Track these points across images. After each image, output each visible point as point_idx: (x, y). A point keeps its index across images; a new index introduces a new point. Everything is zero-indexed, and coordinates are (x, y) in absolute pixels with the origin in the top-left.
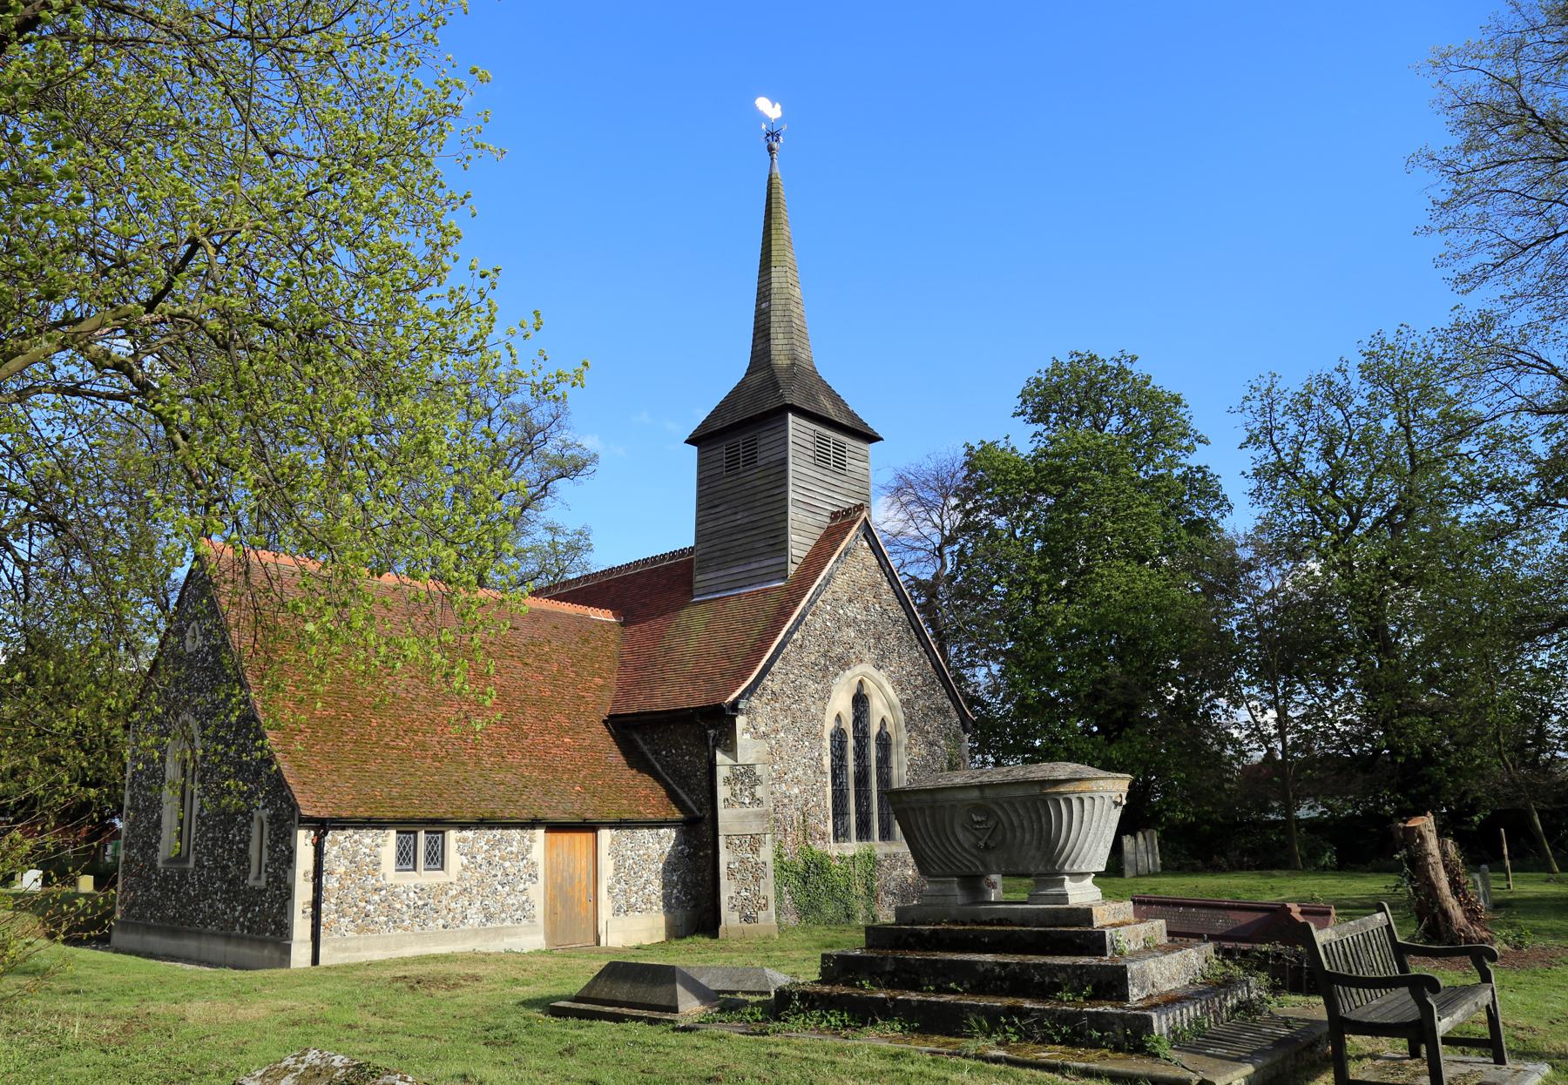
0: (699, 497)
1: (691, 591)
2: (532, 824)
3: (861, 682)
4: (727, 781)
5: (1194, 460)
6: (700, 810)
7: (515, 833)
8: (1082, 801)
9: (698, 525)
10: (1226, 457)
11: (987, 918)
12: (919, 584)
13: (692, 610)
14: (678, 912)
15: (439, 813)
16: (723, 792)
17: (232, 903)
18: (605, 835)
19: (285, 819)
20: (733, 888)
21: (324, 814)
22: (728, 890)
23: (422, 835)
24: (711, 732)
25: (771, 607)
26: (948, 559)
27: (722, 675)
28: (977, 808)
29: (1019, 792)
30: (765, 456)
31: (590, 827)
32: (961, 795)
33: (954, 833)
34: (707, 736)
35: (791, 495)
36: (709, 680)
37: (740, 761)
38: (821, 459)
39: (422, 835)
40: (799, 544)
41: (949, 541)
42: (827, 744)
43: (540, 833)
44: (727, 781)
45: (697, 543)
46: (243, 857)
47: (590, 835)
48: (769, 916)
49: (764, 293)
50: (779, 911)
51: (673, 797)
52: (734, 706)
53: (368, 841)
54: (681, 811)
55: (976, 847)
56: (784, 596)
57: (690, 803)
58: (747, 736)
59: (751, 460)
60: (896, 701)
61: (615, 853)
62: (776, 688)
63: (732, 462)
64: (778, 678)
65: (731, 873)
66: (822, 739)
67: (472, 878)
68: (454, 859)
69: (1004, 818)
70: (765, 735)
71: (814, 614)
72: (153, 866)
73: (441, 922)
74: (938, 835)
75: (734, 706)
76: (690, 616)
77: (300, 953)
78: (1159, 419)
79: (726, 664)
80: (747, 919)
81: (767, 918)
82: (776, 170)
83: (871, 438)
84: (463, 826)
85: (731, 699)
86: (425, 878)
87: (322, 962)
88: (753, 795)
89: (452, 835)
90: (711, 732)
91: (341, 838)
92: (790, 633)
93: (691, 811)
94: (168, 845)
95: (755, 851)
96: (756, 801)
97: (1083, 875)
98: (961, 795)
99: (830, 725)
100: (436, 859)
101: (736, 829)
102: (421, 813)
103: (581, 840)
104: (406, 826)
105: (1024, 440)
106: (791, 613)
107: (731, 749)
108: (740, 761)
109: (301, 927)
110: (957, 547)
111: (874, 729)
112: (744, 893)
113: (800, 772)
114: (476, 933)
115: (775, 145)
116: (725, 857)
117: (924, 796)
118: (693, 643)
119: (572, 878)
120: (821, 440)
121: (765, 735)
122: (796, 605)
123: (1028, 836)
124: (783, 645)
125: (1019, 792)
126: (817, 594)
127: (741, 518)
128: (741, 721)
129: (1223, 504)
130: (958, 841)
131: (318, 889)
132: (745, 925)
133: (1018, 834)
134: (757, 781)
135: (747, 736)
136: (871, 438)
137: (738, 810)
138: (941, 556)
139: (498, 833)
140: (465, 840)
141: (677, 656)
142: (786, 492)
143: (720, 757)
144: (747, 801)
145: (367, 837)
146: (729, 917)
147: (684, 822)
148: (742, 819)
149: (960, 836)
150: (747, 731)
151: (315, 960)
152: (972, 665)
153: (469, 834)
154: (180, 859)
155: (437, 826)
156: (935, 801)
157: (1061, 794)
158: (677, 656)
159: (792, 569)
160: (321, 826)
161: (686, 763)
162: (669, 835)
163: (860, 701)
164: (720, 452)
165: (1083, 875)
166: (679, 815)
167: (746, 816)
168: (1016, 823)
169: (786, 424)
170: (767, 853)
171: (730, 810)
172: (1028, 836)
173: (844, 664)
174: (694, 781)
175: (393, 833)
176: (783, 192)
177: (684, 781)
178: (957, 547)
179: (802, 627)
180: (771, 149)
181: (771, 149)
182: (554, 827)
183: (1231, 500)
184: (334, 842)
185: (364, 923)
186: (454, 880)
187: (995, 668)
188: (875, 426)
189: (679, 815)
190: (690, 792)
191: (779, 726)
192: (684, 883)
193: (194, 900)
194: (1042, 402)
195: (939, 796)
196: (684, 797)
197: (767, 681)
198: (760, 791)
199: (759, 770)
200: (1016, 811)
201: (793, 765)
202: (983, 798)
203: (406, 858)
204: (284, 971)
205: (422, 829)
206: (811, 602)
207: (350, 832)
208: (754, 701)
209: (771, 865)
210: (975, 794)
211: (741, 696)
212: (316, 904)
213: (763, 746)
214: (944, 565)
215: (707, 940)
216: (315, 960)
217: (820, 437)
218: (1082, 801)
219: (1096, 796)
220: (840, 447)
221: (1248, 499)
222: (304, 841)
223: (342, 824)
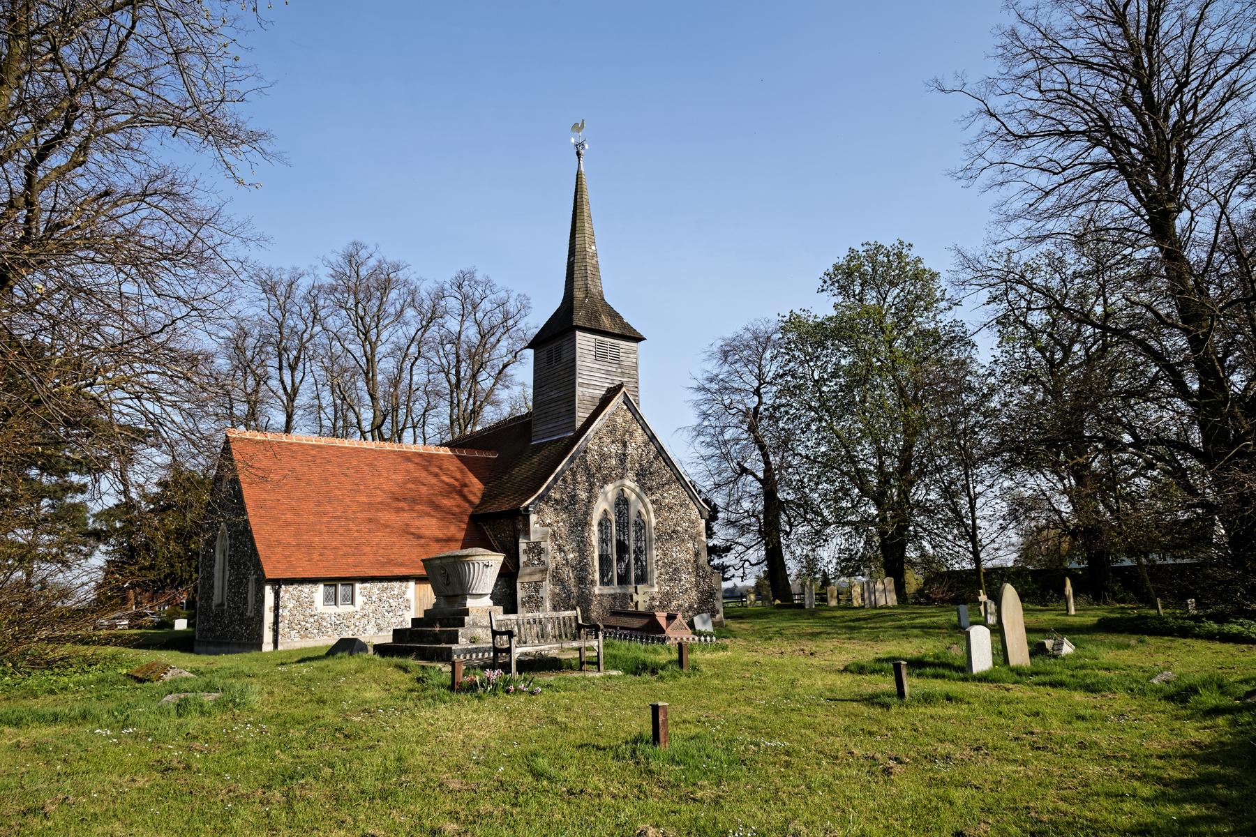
2: (314, 581)
7: (396, 584)
10: (972, 314)
16: (523, 558)
17: (229, 624)
19: (262, 581)
30: (565, 357)
40: (581, 415)
43: (412, 584)
44: (525, 552)
46: (246, 603)
59: (559, 359)
65: (524, 604)
68: (359, 599)
72: (210, 606)
77: (267, 646)
83: (639, 339)
84: (364, 580)
86: (344, 609)
89: (358, 586)
94: (216, 599)
97: (481, 595)
104: (330, 582)
105: (824, 307)
107: (527, 533)
109: (268, 636)
115: (582, 152)
128: (533, 518)
131: (276, 616)
136: (639, 339)
139: (385, 584)
145: (306, 588)
153: (368, 585)
154: (222, 604)
160: (277, 583)
165: (481, 595)
175: (321, 586)
176: (587, 184)
180: (578, 154)
181: (578, 154)
184: (286, 591)
193: (227, 626)
194: (845, 276)
199: (543, 545)
203: (327, 599)
204: (254, 654)
212: (276, 623)
222: (269, 592)
223: (290, 582)
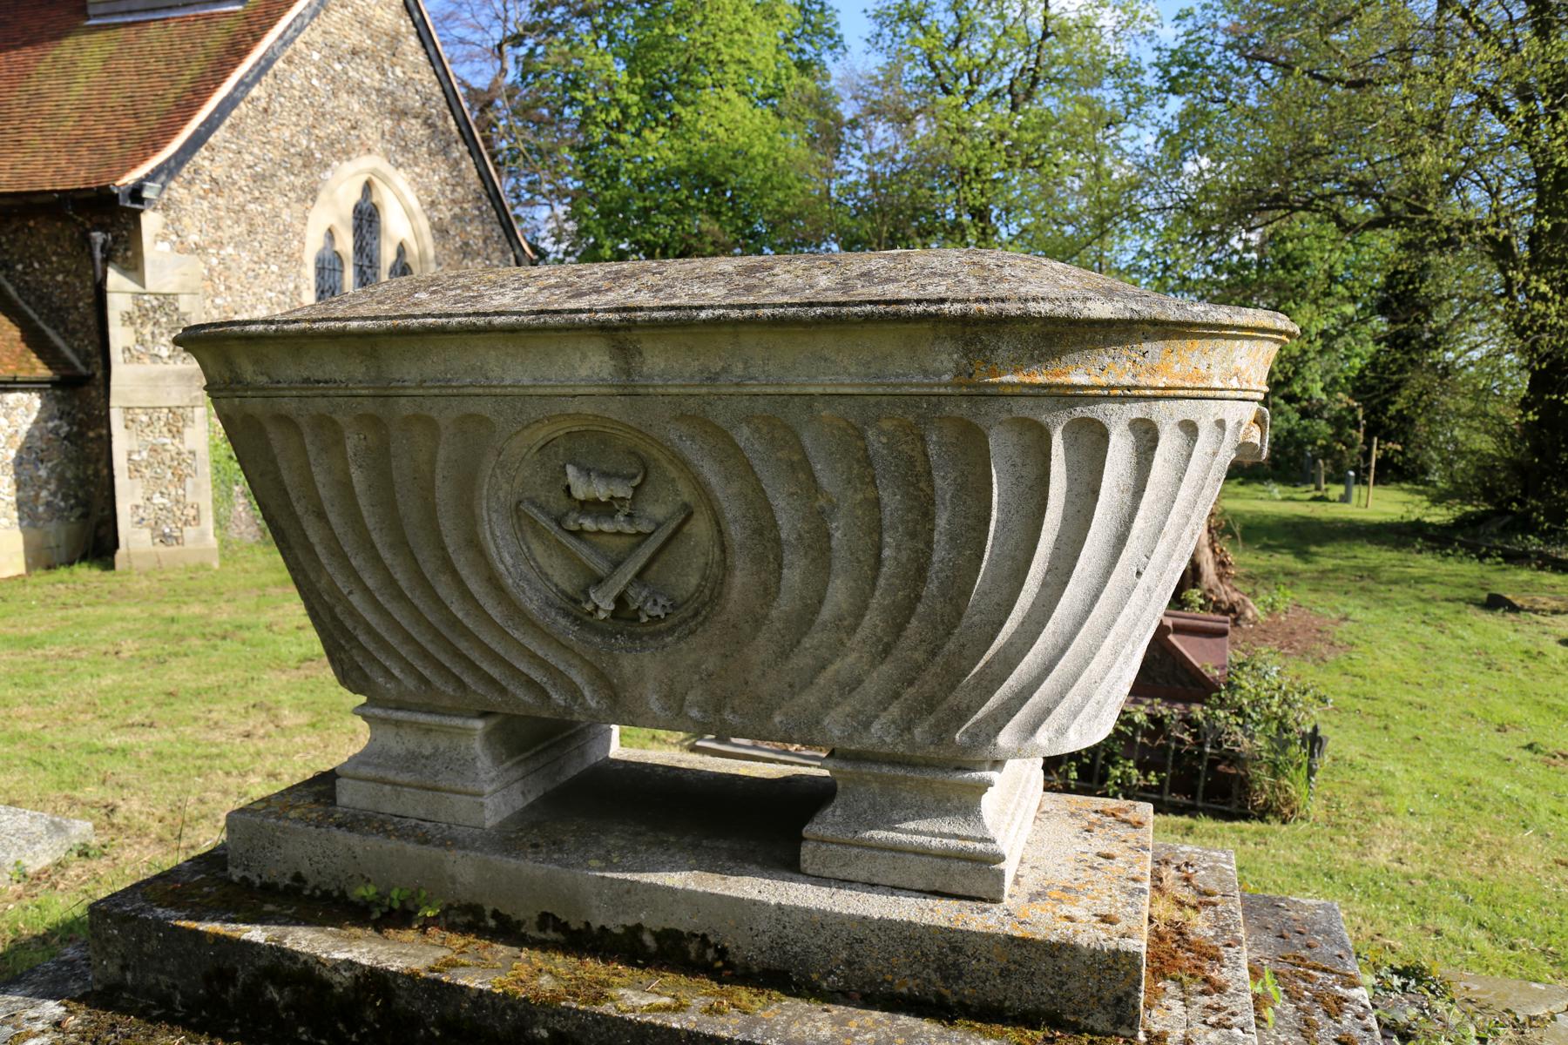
1: (85, 8)
3: (368, 187)
4: (128, 319)
6: (87, 365)
8: (1146, 436)
11: (617, 923)
12: (473, 93)
13: (84, 39)
14: (53, 526)
16: (120, 336)
20: (139, 492)
22: (129, 496)
24: (98, 237)
25: (217, 40)
26: (510, 64)
27: (121, 141)
28: (587, 443)
29: (837, 372)
32: (513, 370)
33: (474, 544)
34: (87, 242)
36: (100, 149)
41: (517, 40)
42: (310, 272)
44: (128, 319)
48: (203, 535)
50: (220, 523)
51: (35, 340)
52: (136, 193)
54: (49, 365)
55: (573, 606)
56: (238, 26)
57: (68, 352)
58: (165, 247)
62: (219, 173)
64: (223, 158)
65: (135, 469)
66: (300, 262)
69: (726, 493)
70: (198, 249)
71: (289, 61)
74: (402, 544)
75: (136, 193)
76: (80, 48)
79: (130, 125)
80: (165, 539)
81: (203, 537)
85: (130, 178)
90: (98, 237)
92: (244, 85)
93: (68, 364)
95: (177, 433)
98: (513, 370)
99: (314, 244)
101: (141, 397)
106: (247, 52)
107: (134, 267)
110: (523, 51)
111: (388, 255)
112: (157, 499)
116: (122, 443)
117: (334, 367)
118: (79, 89)
121: (198, 249)
122: (257, 39)
123: (839, 593)
124: (230, 103)
125: (837, 372)
126: (298, 28)
128: (151, 222)
129: (835, 42)
130: (494, 582)
132: (162, 548)
133: (793, 576)
135: (165, 247)
137: (148, 368)
138: (501, 56)
141: (47, 107)
143: (114, 278)
146: (132, 536)
147: (54, 384)
148: (154, 381)
149: (505, 559)
152: (531, 203)
156: (386, 394)
157: (1069, 396)
158: (47, 107)
161: (57, 285)
162: (34, 401)
163: (366, 218)
167: (162, 377)
168: (788, 523)
171: (135, 368)
172: (839, 593)
173: (341, 149)
174: (74, 316)
177: (57, 316)
178: (523, 51)
179: (267, 79)
183: (846, 41)
187: (560, 210)
189: (43, 371)
190: (68, 334)
191: (224, 235)
192: (62, 480)
195: (407, 370)
196: (58, 341)
197: (201, 157)
200: (801, 467)
201: (250, 300)
202: (630, 393)
206: (285, 41)
208: (176, 189)
210: (593, 365)
211: (152, 176)
213: (197, 266)
214: (504, 71)
215: (96, 572)
218: (1146, 436)
219: (1167, 416)
221: (865, 46)
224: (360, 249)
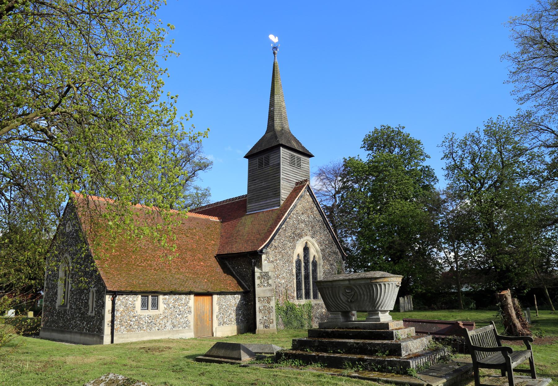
0: (249, 177)
1: (246, 210)
2: (189, 293)
3: (306, 243)
4: (259, 278)
5: (425, 164)
6: (249, 288)
7: (183, 297)
8: (385, 285)
9: (248, 187)
10: (436, 163)
11: (351, 327)
12: (327, 208)
13: (246, 217)
14: (241, 325)
15: (156, 289)
16: (257, 282)
17: (82, 321)
18: (215, 297)
19: (102, 291)
20: (261, 316)
21: (115, 290)
22: (259, 317)
23: (150, 297)
24: (253, 260)
25: (274, 216)
26: (337, 199)
27: (257, 240)
28: (348, 287)
29: (363, 282)
30: (272, 162)
31: (210, 294)
32: (342, 283)
33: (339, 296)
34: (251, 262)
35: (282, 176)
36: (252, 242)
37: (263, 271)
38: (292, 163)
39: (150, 297)
40: (284, 194)
41: (338, 192)
42: (294, 265)
43: (192, 296)
44: (259, 278)
45: (248, 193)
46: (86, 305)
47: (210, 297)
48: (274, 326)
49: (272, 104)
50: (277, 324)
51: (240, 283)
52: (261, 251)
53: (131, 299)
54: (242, 288)
55: (347, 301)
56: (279, 212)
57: (245, 286)
58: (266, 262)
59: (267, 164)
60: (319, 249)
61: (219, 304)
62: (276, 245)
63: (261, 164)
64: (277, 241)
65: (260, 311)
66: (292, 263)
67: (168, 312)
68: (162, 306)
69: (357, 291)
70: (272, 262)
71: (290, 219)
72: (55, 308)
73: (157, 328)
74: (334, 297)
75: (261, 251)
76: (246, 219)
77: (107, 339)
78: (413, 149)
79: (258, 236)
80: (266, 327)
81: (273, 327)
82: (276, 60)
83: (310, 156)
84: (165, 294)
85: (260, 249)
86: (151, 312)
87: (115, 342)
88: (268, 283)
89: (161, 297)
90: (253, 260)
91: (121, 298)
92: (281, 225)
93: (246, 289)
94: (60, 301)
95: (269, 303)
96: (269, 285)
97: (386, 311)
98: (342, 283)
99: (295, 258)
100: (155, 306)
101: (262, 295)
102: (150, 289)
103: (207, 299)
104: (145, 294)
105: (364, 156)
106: (282, 218)
107: (260, 267)
108: (263, 271)
109: (107, 330)
110: (340, 195)
111: (311, 259)
112: (265, 318)
113: (285, 275)
114: (169, 332)
115: (276, 52)
116: (258, 305)
117: (329, 283)
118: (247, 229)
119: (203, 312)
120: (292, 156)
121: (272, 262)
122: (283, 215)
123: (366, 297)
124: (278, 229)
125: (363, 282)
126: (291, 211)
127: (264, 184)
128: (264, 257)
129: (435, 179)
130: (341, 299)
131: (113, 316)
132: (265, 329)
133: (362, 297)
134: (269, 278)
135: (266, 262)
136: (310, 156)
137: (263, 288)
138: (335, 198)
139: (177, 296)
140: (165, 299)
141: (241, 233)
142: (280, 175)
143: (256, 269)
144: (266, 285)
145: (131, 298)
146: (260, 326)
147: (243, 293)
148: (264, 291)
149: (342, 298)
150: (266, 260)
151: (112, 341)
152: (346, 237)
153: (167, 297)
154: (64, 305)
155: (156, 294)
156: (333, 285)
157: (377, 282)
158: (241, 233)
159: (282, 202)
160: (114, 294)
161: (244, 271)
162: (238, 297)
163: (306, 249)
164: (256, 161)
165: (386, 311)
166: (242, 290)
167: (266, 290)
168: (362, 293)
169: (280, 151)
170: (273, 304)
171: (260, 288)
172: (366, 297)
173: (300, 236)
174: (247, 278)
175: (140, 296)
176: (279, 68)
177: (243, 278)
178: (340, 195)
179: (286, 223)
180: (274, 53)
181: (274, 53)
182: (197, 294)
183: (438, 178)
184: (119, 300)
185: (130, 328)
186: (162, 313)
187: (354, 238)
188: (311, 152)
189: (242, 290)
190: (246, 282)
191: (277, 258)
192: (243, 314)
193: (69, 320)
194: (371, 143)
195: (334, 283)
196: (244, 283)
197: (273, 242)
198: (270, 282)
199: (270, 274)
200: (362, 288)
201: (282, 272)
202: (350, 284)
203: (144, 305)
204: (101, 345)
205: (150, 295)
206: (289, 214)
207: (125, 296)
208: (268, 250)
209: (274, 308)
210: (347, 282)
211: (264, 248)
212: (113, 322)
213: (272, 265)
214: (336, 201)
215: (252, 334)
216: (112, 341)
217: (292, 155)
218: (385, 285)
219: (390, 283)
220: (299, 159)
221: (444, 178)
222: (108, 299)
223: (122, 293)
224: (305, 256)
